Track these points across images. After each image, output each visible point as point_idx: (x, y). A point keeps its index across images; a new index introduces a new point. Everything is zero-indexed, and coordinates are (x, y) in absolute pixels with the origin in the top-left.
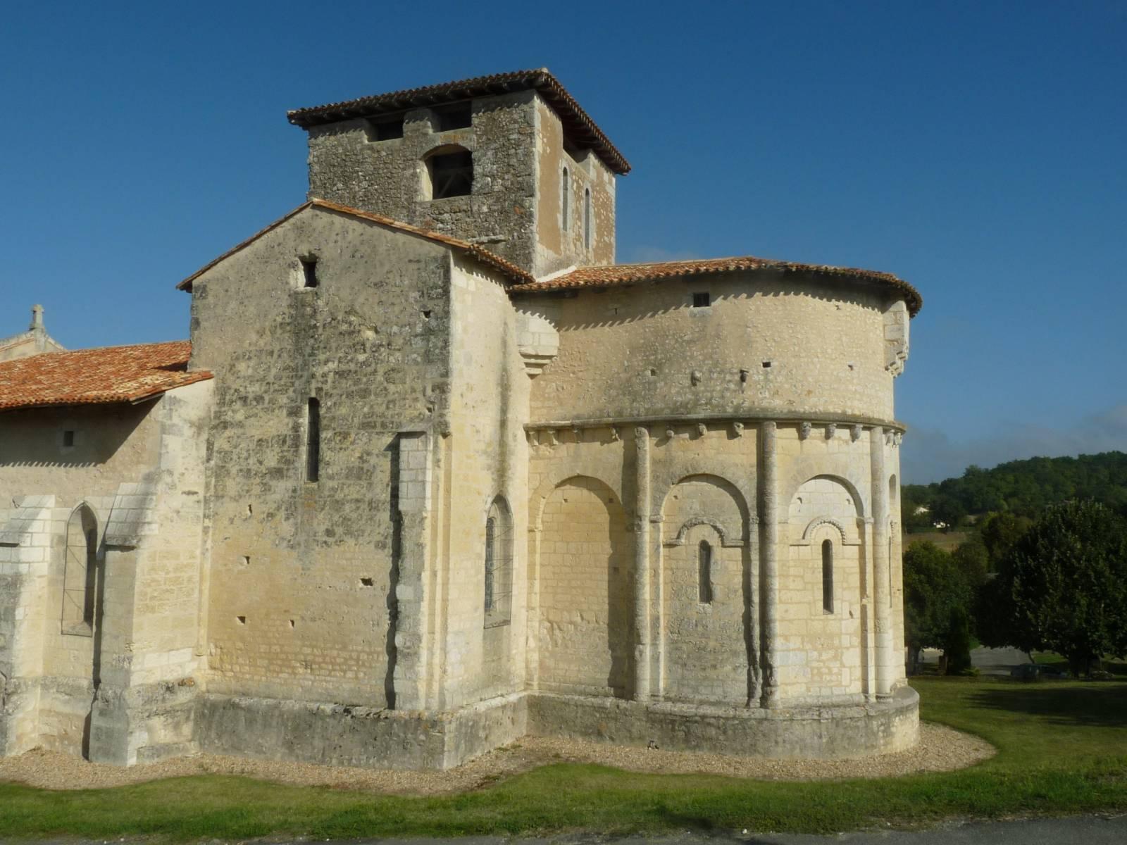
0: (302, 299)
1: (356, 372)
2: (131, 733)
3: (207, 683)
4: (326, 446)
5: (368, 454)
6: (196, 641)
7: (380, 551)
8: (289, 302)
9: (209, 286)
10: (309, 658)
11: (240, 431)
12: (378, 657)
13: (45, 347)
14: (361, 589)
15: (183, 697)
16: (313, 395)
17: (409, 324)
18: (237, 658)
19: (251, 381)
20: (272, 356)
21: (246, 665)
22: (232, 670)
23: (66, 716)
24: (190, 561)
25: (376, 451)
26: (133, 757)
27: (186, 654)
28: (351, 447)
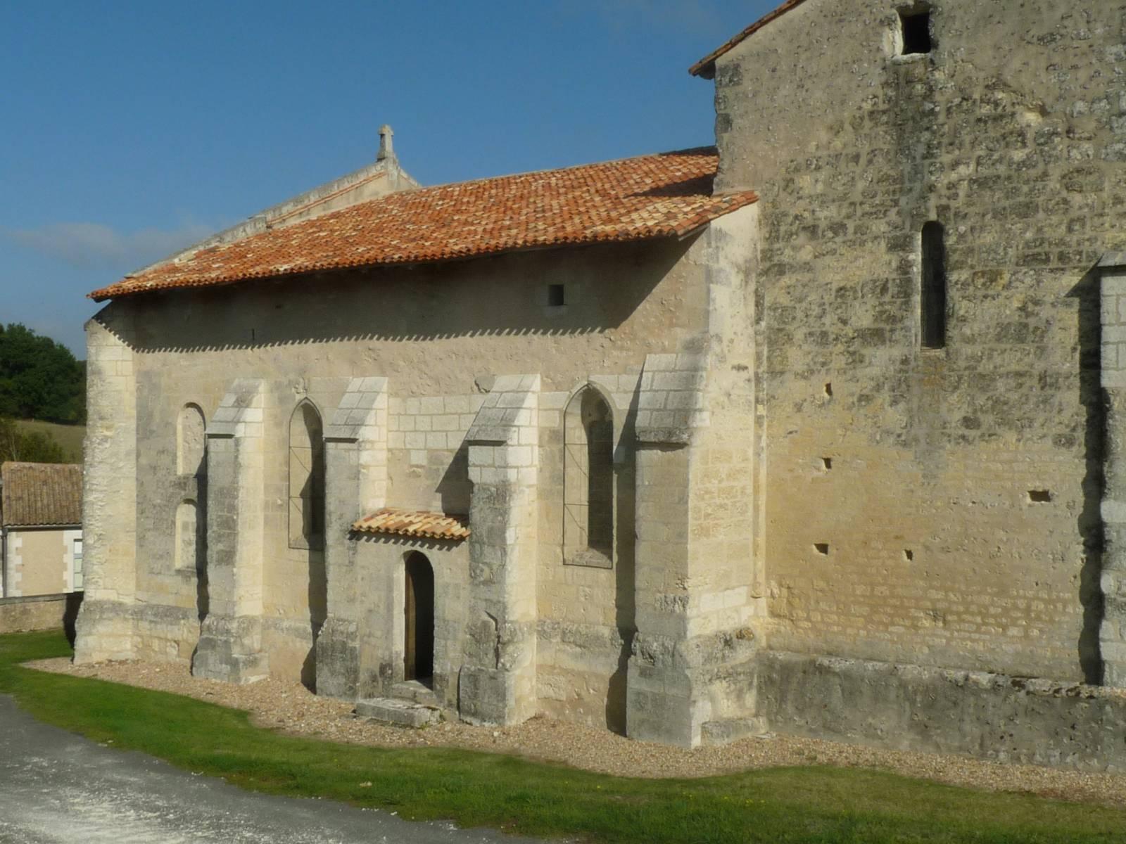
0: (907, 73)
1: (1009, 178)
2: (695, 702)
3: (768, 636)
4: (959, 294)
5: (1037, 303)
6: (751, 577)
7: (1063, 450)
8: (883, 79)
9: (744, 66)
10: (940, 605)
11: (808, 276)
12: (1065, 607)
13: (399, 184)
14: (1030, 506)
15: (743, 654)
16: (933, 216)
17: (1107, 97)
18: (817, 602)
19: (823, 202)
20: (857, 163)
21: (832, 613)
22: (808, 619)
23: (580, 674)
24: (743, 465)
25: (1050, 298)
26: (697, 735)
27: (740, 595)
28: (1004, 293)
